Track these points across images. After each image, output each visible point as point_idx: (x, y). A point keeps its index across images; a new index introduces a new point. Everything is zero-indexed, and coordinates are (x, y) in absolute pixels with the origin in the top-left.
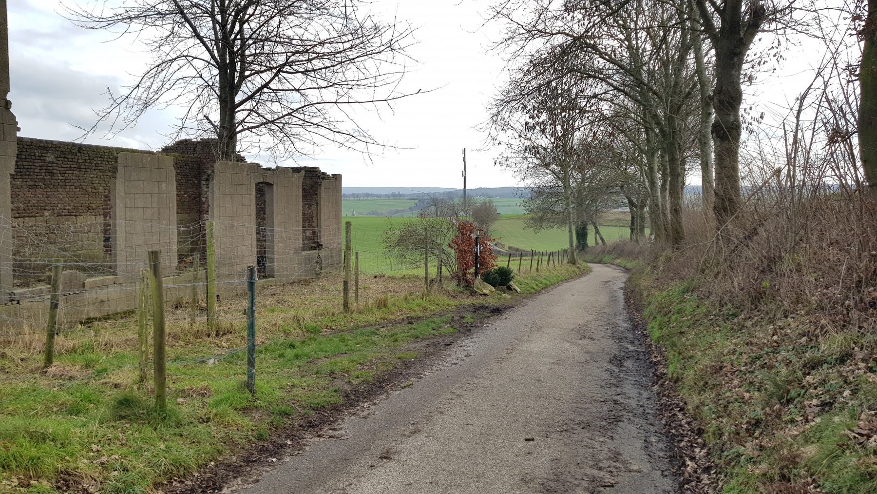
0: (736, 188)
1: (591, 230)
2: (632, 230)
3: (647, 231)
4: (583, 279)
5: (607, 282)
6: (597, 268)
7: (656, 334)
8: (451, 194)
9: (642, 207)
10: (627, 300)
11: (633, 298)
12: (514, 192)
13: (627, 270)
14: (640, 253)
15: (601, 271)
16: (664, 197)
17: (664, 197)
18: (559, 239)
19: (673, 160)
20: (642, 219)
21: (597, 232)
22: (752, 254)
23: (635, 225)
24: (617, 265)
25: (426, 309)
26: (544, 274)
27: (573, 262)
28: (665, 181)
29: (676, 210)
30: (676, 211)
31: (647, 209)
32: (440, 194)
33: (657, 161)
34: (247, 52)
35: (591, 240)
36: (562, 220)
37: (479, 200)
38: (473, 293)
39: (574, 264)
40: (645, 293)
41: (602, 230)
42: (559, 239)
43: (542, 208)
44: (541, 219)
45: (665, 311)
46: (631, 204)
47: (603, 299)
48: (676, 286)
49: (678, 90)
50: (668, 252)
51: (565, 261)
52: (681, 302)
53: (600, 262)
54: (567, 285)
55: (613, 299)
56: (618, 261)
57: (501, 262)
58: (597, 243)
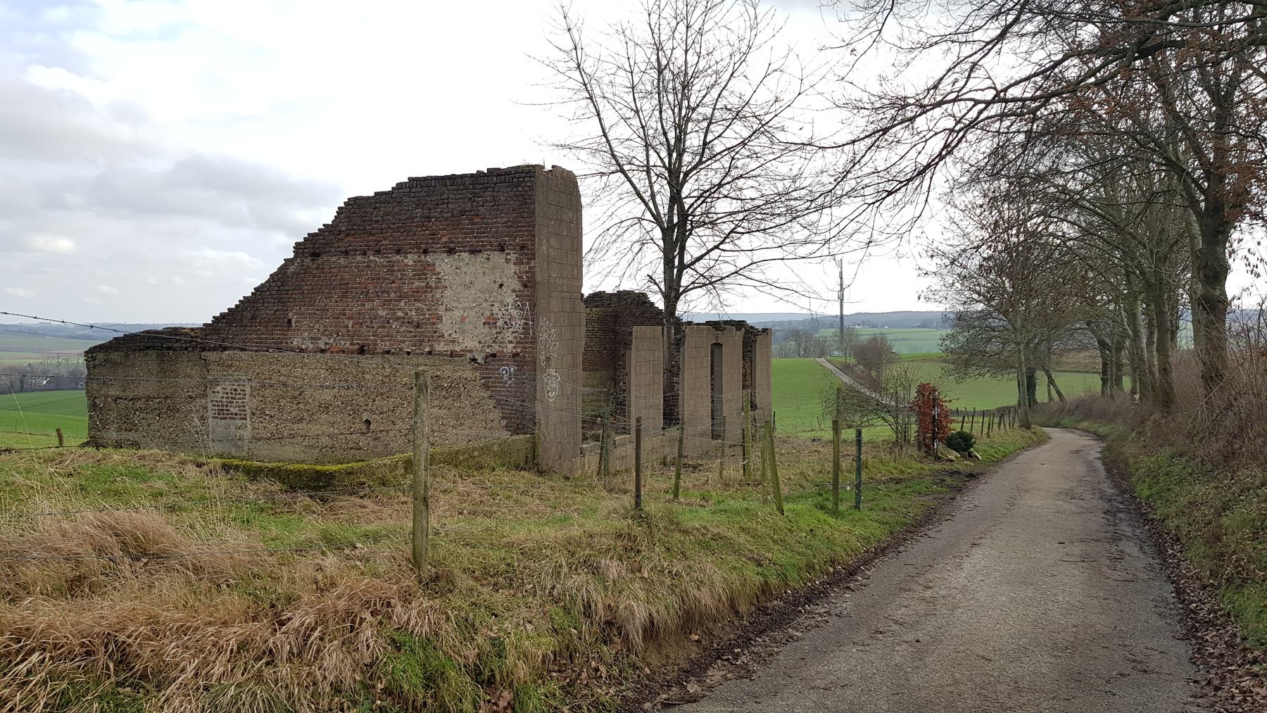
0: (1222, 359)
1: (1041, 377)
2: (1104, 381)
3: (1127, 383)
4: (1044, 447)
5: (1077, 452)
6: (1054, 433)
7: (1146, 493)
8: (816, 322)
9: (1119, 349)
10: (1109, 470)
11: (1115, 466)
12: (924, 321)
13: (1100, 437)
14: (1116, 414)
15: (1063, 439)
16: (1150, 352)
17: (1150, 352)
18: (1005, 392)
19: (1160, 313)
20: (1119, 366)
21: (1051, 382)
22: (1229, 422)
23: (1109, 374)
24: (1083, 430)
25: (902, 472)
26: (997, 440)
27: (1026, 425)
28: (1151, 333)
29: (1165, 369)
30: (1165, 370)
31: (1124, 353)
32: (799, 322)
33: (1141, 307)
34: (685, 192)
35: (1041, 394)
36: (999, 365)
37: (865, 334)
38: (938, 459)
39: (1028, 428)
40: (1131, 461)
41: (1059, 379)
42: (1002, 391)
43: (971, 345)
44: (967, 364)
45: (1154, 475)
46: (1103, 345)
47: (1080, 469)
48: (1166, 451)
49: (1164, 237)
50: (1157, 416)
51: (1016, 425)
52: (1170, 466)
53: (1056, 425)
54: (1028, 454)
55: (1092, 469)
56: (1085, 424)
57: (955, 427)
58: (1051, 399)
